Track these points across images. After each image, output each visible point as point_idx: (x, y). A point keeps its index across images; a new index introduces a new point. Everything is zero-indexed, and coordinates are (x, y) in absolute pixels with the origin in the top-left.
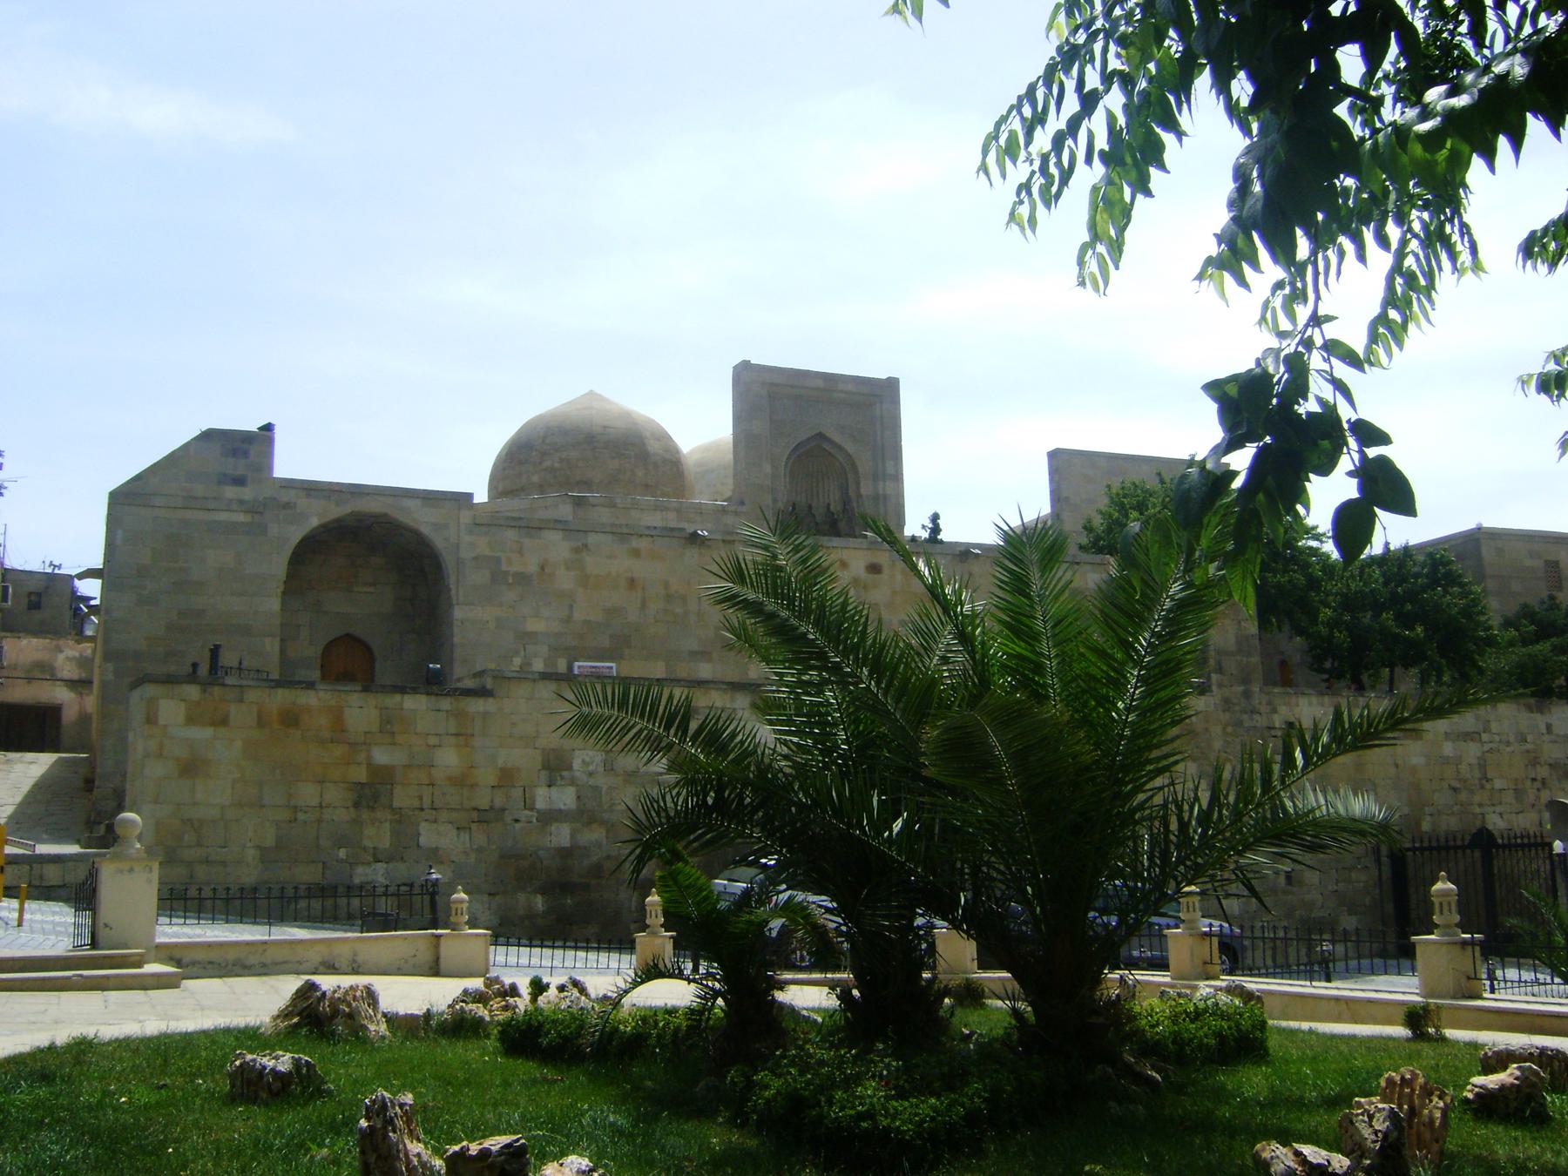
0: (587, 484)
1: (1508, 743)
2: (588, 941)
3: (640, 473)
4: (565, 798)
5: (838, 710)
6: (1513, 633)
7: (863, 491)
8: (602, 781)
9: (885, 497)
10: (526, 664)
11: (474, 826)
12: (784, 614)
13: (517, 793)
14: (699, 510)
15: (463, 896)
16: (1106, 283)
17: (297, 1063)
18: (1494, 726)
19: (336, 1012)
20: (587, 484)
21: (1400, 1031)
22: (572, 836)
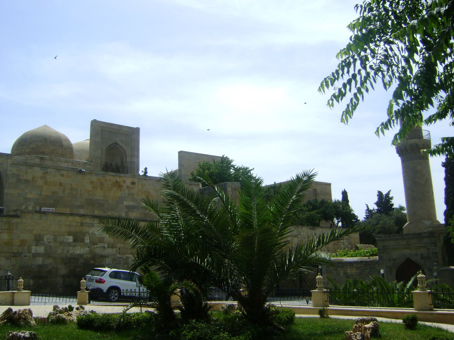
0: (44, 153)
1: (305, 238)
2: (46, 294)
3: (60, 151)
4: (41, 249)
5: (182, 227)
6: (306, 208)
7: (127, 160)
8: (52, 244)
9: (134, 162)
10: (26, 208)
11: (12, 258)
12: (185, 200)
13: (26, 248)
14: (78, 163)
15: (22, 280)
16: (347, 122)
17: (30, 334)
18: (302, 234)
19: (20, 318)
20: (44, 153)
21: (318, 316)
22: (43, 261)
